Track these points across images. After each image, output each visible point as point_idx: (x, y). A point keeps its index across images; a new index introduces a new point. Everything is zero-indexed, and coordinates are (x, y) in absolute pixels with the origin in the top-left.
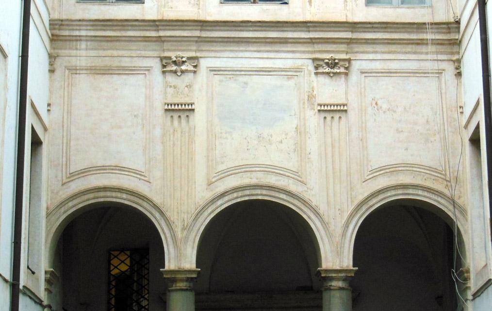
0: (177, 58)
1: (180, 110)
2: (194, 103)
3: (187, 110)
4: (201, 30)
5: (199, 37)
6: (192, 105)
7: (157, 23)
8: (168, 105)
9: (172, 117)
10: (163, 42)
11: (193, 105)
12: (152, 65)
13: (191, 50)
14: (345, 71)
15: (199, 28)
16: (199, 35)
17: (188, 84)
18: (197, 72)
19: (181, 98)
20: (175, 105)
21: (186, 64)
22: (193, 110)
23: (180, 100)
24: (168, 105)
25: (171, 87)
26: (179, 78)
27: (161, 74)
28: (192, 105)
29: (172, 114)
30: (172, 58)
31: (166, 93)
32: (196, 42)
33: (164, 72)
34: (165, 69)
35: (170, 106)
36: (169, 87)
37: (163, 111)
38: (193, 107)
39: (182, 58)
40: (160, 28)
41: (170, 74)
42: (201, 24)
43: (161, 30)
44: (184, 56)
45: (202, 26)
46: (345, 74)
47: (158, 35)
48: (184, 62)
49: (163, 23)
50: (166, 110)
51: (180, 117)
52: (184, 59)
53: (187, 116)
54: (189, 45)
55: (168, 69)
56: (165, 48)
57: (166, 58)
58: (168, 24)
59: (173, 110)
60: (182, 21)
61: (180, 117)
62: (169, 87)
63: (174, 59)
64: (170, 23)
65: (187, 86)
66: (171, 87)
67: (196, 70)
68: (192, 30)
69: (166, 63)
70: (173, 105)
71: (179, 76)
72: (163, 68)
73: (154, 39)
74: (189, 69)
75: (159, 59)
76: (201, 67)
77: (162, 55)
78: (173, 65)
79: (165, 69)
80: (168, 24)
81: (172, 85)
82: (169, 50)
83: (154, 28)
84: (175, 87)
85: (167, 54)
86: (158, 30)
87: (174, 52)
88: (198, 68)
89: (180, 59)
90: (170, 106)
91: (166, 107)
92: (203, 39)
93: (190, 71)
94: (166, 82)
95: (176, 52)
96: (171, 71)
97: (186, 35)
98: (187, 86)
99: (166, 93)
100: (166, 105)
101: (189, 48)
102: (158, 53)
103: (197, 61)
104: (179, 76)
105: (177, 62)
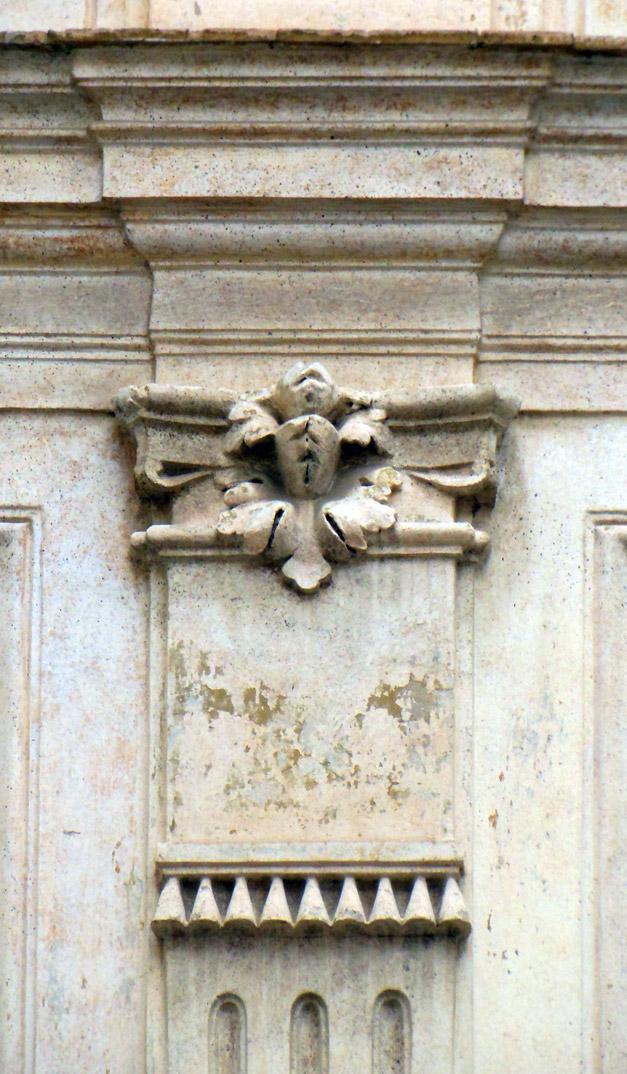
0: (280, 419)
1: (312, 933)
2: (459, 870)
3: (386, 935)
4: (533, 143)
5: (513, 211)
6: (436, 886)
7: (86, 71)
8: (189, 886)
9: (229, 1004)
10: (142, 261)
11: (451, 887)
12: (29, 495)
13: (430, 346)
14: (464, 527)
15: (516, 117)
16: (511, 190)
17: (398, 678)
18: (495, 560)
19: (329, 815)
20: (260, 886)
21: (377, 474)
22: (453, 935)
23: (315, 831)
24: (189, 886)
25: (218, 702)
26: (301, 612)
27: (119, 581)
28: (436, 886)
29: (227, 973)
30: (235, 413)
31: (165, 767)
32: (487, 259)
33: (148, 562)
34: (158, 531)
35: (206, 898)
36: (194, 706)
37: (145, 937)
38: (453, 904)
39: (341, 412)
40: (114, 116)
41: (209, 572)
42: (535, 76)
43: (122, 136)
44: (358, 395)
45: (540, 99)
46: (461, 564)
47: (90, 196)
48: (356, 457)
49: (143, 72)
50: (170, 937)
51: (310, 1005)
52: (359, 429)
53: (392, 1001)
54: (405, 300)
55: (194, 523)
56: (159, 322)
57: (168, 414)
58: (195, 75)
59: (240, 936)
60: (342, 47)
61: (310, 1005)
62: (194, 706)
63: (260, 425)
64: (225, 73)
65: (387, 699)
66: (218, 702)
67: (480, 536)
68: (449, 136)
69: (170, 469)
70: (385, 889)
71: (302, 594)
72: (143, 520)
73: (56, 234)
74: (405, 526)
75: (99, 431)
76: (535, 507)
77: (136, 384)
78: (250, 488)
79: (158, 531)
80: (195, 75)
81: (233, 684)
82: (201, 344)
83: (57, 125)
84: (262, 709)
85: (178, 381)
86: (91, 146)
87: (255, 368)
88: (502, 521)
89: (320, 425)
90: (206, 898)
91: (170, 905)
92: (557, 237)
93: (421, 549)
94: (174, 661)
95: (276, 365)
96: (225, 549)
97: (380, 188)
98: (387, 699)
99: (165, 767)
100: (173, 889)
101: (414, 322)
102: (93, 372)
103: (490, 441)
104: (302, 594)
105: (289, 452)
